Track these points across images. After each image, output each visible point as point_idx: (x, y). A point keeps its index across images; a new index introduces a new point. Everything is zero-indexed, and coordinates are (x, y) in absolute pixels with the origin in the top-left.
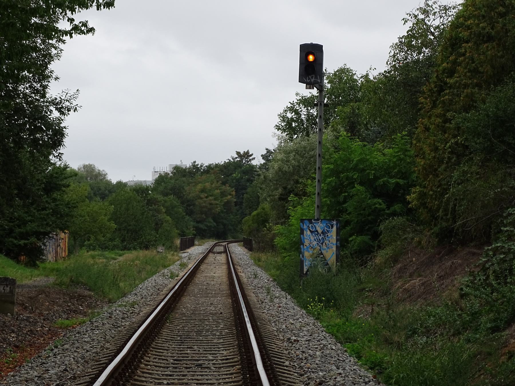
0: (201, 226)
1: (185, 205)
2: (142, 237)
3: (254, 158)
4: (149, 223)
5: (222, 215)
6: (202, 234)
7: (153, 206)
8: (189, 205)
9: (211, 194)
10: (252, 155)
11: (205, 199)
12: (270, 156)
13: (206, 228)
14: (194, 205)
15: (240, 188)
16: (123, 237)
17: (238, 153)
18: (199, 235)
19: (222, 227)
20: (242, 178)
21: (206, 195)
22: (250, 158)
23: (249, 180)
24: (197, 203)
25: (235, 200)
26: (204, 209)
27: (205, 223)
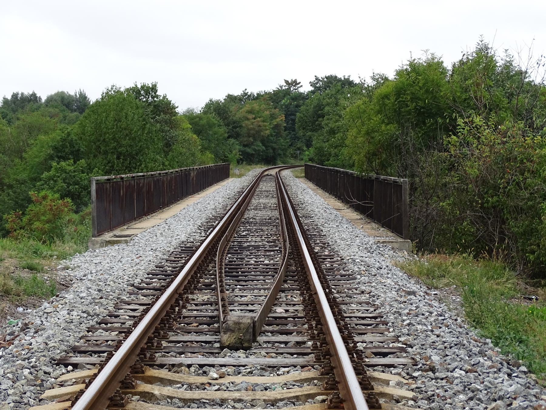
0: (249, 150)
1: (231, 127)
2: (140, 165)
3: (302, 86)
4: (154, 142)
5: (272, 138)
6: (248, 159)
7: (162, 115)
8: (235, 127)
9: (259, 116)
10: (300, 83)
11: (253, 121)
12: (318, 83)
13: (254, 153)
14: (241, 127)
15: (289, 114)
16: (110, 165)
17: (287, 82)
18: (246, 160)
19: (271, 151)
20: (291, 104)
21: (254, 116)
22: (298, 86)
23: (298, 106)
24: (244, 125)
25: (285, 125)
26: (252, 132)
27: (253, 147)
